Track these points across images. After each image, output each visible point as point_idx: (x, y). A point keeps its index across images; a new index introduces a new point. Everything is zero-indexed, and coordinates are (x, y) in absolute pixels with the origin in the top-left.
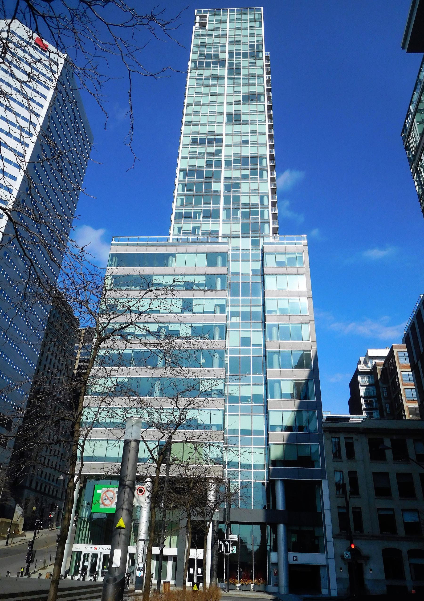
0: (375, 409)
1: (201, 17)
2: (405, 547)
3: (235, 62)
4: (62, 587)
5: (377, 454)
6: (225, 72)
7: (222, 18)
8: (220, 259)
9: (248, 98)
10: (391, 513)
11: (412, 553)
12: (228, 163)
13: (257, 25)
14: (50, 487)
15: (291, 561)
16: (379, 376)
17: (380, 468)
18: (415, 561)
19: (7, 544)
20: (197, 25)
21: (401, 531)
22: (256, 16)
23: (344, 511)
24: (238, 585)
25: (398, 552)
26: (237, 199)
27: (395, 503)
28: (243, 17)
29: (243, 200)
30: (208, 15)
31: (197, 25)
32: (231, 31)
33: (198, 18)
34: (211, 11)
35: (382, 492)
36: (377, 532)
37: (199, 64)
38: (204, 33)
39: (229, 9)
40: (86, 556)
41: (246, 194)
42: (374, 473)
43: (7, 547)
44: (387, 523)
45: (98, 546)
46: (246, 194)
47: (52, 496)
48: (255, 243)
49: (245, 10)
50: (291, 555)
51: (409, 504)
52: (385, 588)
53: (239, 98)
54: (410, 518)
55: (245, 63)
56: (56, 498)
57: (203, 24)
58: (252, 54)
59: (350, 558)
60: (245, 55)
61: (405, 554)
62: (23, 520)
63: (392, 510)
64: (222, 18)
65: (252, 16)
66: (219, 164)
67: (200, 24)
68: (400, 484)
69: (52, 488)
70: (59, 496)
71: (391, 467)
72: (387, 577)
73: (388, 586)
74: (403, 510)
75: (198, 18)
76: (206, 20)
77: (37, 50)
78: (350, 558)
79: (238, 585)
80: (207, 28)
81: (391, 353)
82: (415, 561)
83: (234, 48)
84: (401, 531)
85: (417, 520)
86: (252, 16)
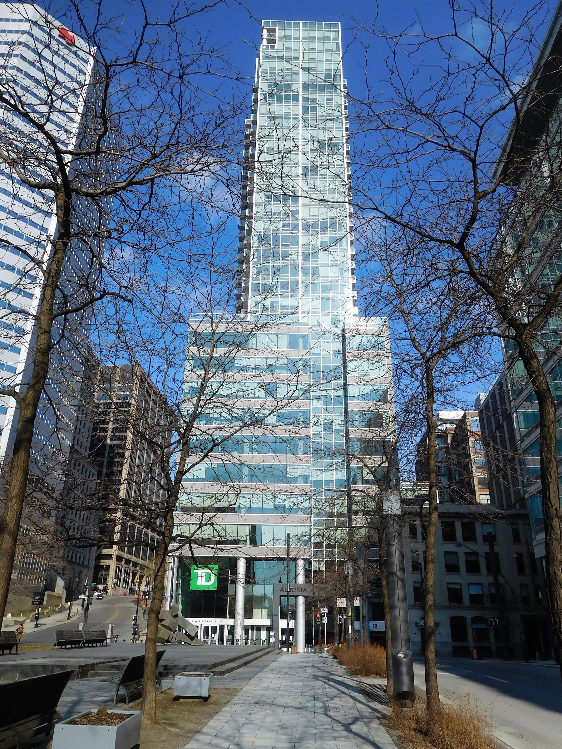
0: (444, 475)
1: (269, 31)
2: (469, 615)
3: (310, 97)
4: (449, 628)
5: (448, 535)
6: (298, 109)
7: (293, 33)
8: (301, 340)
9: (326, 146)
10: (458, 586)
11: (475, 620)
12: (306, 228)
13: (334, 47)
14: (76, 555)
15: (372, 628)
16: (449, 442)
17: (451, 547)
18: (477, 626)
19: (69, 617)
20: (265, 42)
21: (466, 601)
22: (333, 35)
23: (418, 585)
24: (326, 649)
25: (464, 619)
26: (315, 271)
27: (462, 578)
28: (319, 34)
29: (322, 271)
30: (277, 29)
31: (265, 42)
32: (303, 54)
33: (265, 31)
34: (282, 24)
35: (452, 568)
36: (446, 603)
37: (270, 96)
38: (273, 54)
39: (301, 22)
40: (214, 628)
41: (325, 265)
42: (445, 553)
43: (69, 621)
44: (455, 595)
45: (198, 619)
46: (325, 265)
47: (78, 564)
48: (335, 322)
49: (320, 25)
50: (372, 623)
51: (474, 578)
52: (451, 649)
53: (317, 145)
54: (474, 590)
55: (321, 98)
56: (83, 566)
57: (272, 42)
58: (329, 87)
59: (3, 629)
60: (321, 88)
61: (469, 621)
62: (65, 592)
63: (460, 584)
64: (293, 33)
65: (327, 34)
66: (295, 227)
67: (269, 41)
68: (467, 562)
69: (78, 555)
70: (86, 563)
71: (461, 550)
72: (454, 639)
73: (453, 647)
74: (469, 584)
75: (265, 31)
76: (275, 36)
77: (62, 44)
78: (3, 629)
79: (326, 649)
80: (276, 47)
81: (465, 416)
82: (477, 626)
83: (308, 78)
84: (466, 601)
85: (481, 592)
86: (327, 34)
